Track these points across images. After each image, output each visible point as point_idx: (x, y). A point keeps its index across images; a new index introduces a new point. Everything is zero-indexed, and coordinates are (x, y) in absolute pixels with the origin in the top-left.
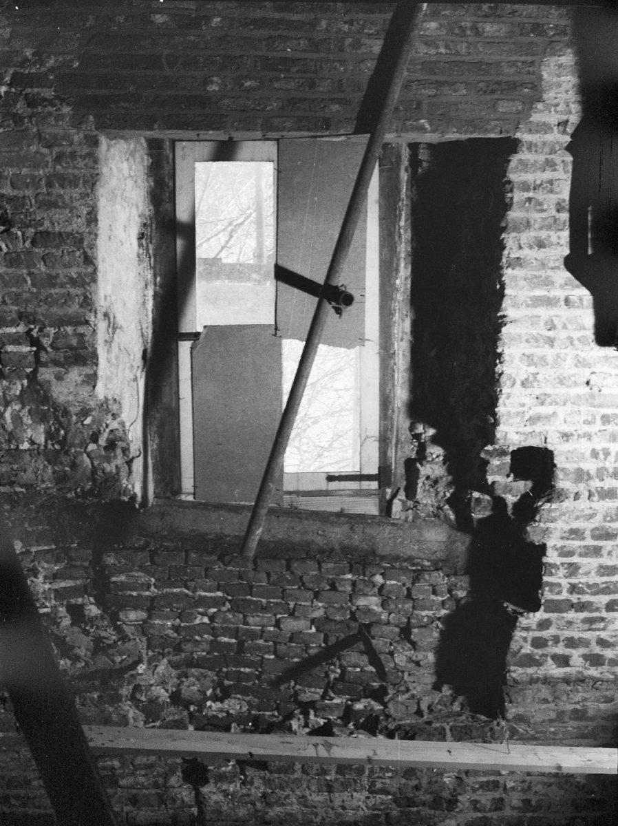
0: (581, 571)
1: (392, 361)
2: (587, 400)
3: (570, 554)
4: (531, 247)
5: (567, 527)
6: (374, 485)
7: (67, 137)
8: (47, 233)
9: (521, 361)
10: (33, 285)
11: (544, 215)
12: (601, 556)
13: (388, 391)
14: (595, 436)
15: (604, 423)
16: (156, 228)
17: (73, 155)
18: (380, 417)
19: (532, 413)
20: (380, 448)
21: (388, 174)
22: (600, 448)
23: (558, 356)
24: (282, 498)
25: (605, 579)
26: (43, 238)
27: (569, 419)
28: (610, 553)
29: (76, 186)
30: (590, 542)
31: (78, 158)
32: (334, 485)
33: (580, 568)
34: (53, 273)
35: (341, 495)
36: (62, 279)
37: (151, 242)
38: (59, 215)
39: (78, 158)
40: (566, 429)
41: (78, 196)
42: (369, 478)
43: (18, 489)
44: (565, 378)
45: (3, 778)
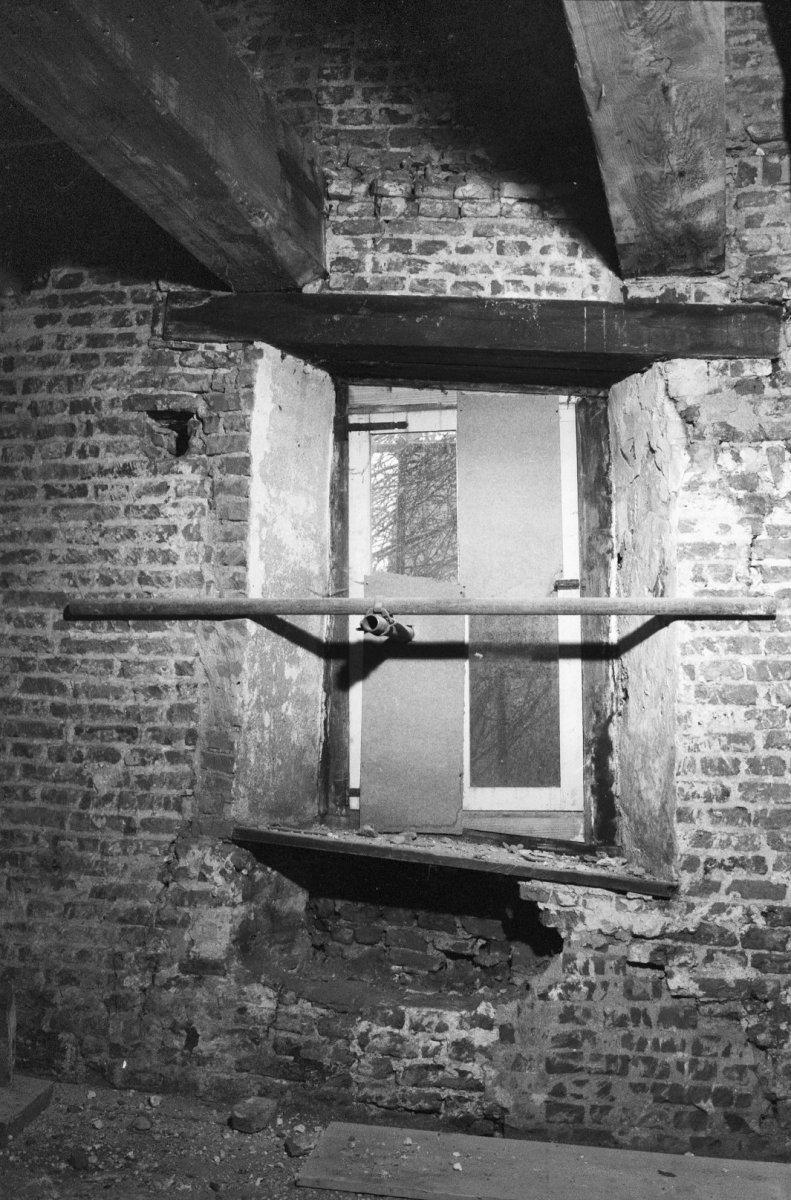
0: (110, 318)
1: (334, 559)
2: (103, 513)
3: (122, 337)
4: (166, 687)
5: (126, 367)
6: (353, 419)
7: (716, 820)
8: (740, 702)
9: (177, 557)
10: (757, 640)
11: (150, 725)
12: (88, 336)
13: (339, 525)
14: (95, 471)
15: (85, 486)
16: (606, 710)
17: (708, 798)
18: (347, 496)
19: (164, 497)
20: (348, 461)
21: (339, 772)
22: (90, 458)
23: (135, 562)
24: (459, 401)
25: (83, 311)
26: (745, 698)
27: (123, 490)
28: (79, 340)
29: (703, 761)
30: (101, 351)
31: (702, 795)
32: (399, 418)
33: (112, 322)
34: (731, 656)
35: (391, 406)
36: (721, 647)
37: (612, 694)
38: (726, 726)
39: (702, 795)
40: (125, 480)
41: (701, 748)
42: (359, 427)
43: (783, 800)
44: (128, 538)
45: (789, 653)
